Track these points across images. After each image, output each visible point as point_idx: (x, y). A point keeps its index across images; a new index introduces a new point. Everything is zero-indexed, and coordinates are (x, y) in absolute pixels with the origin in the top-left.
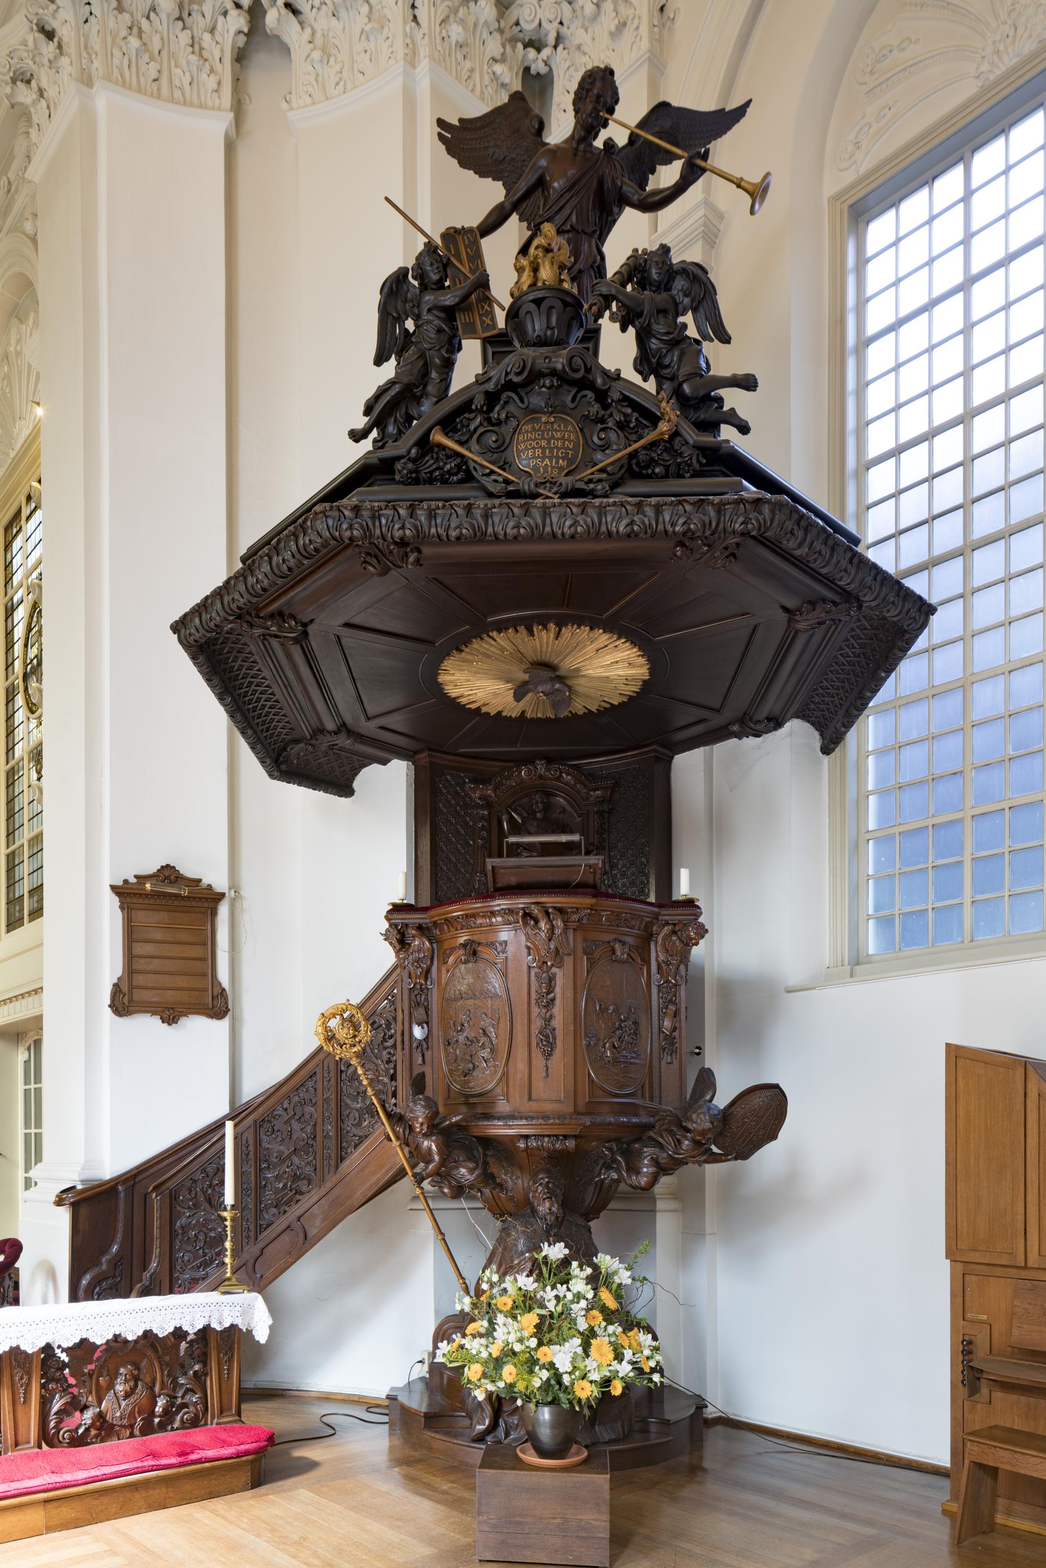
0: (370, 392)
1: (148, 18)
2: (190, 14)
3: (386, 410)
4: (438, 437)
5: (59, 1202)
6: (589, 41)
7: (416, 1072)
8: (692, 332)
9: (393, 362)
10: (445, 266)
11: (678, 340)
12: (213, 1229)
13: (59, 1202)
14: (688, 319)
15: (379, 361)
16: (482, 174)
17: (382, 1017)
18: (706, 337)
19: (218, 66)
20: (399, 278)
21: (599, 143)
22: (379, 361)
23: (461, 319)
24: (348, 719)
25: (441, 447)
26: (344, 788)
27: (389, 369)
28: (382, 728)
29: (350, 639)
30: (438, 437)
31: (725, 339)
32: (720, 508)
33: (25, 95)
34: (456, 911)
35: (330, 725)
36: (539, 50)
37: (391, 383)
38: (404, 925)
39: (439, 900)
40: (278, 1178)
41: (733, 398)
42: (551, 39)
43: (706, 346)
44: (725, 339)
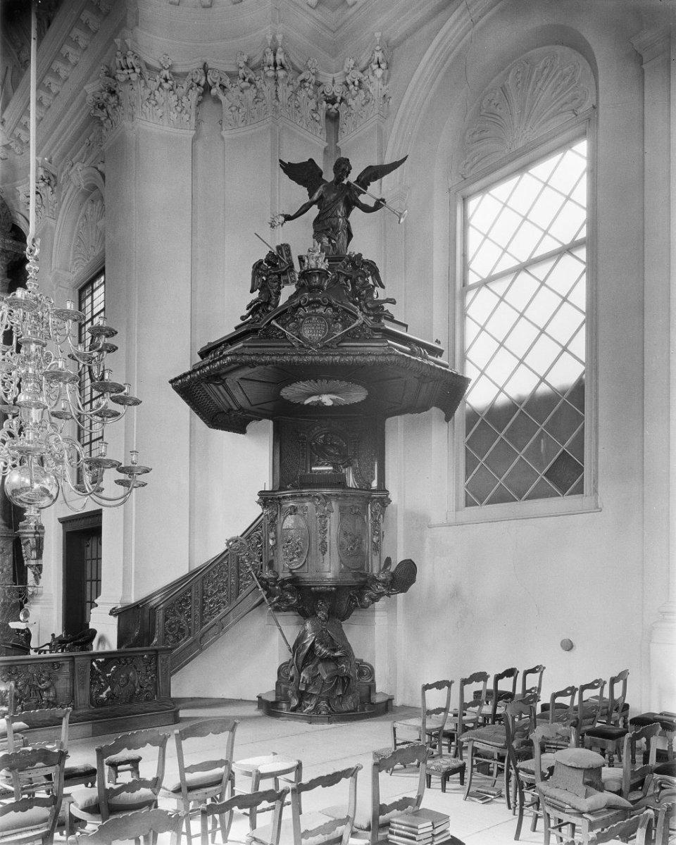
0: (249, 302)
1: (158, 90)
2: (177, 87)
3: (255, 308)
4: (274, 322)
5: (111, 613)
6: (354, 104)
7: (270, 559)
8: (371, 282)
9: (258, 291)
10: (277, 258)
11: (365, 285)
12: (182, 625)
13: (111, 613)
14: (370, 278)
15: (252, 291)
16: (299, 184)
17: (254, 534)
18: (377, 286)
19: (189, 110)
20: (260, 263)
21: (345, 182)
22: (252, 291)
23: (283, 278)
24: (243, 405)
25: (275, 326)
26: (243, 431)
27: (256, 295)
28: (259, 408)
29: (245, 385)
30: (274, 322)
31: (383, 287)
32: (44, 672)
33: (101, 114)
34: (288, 493)
35: (235, 408)
36: (333, 104)
37: (256, 301)
38: (266, 499)
39: (281, 489)
40: (211, 603)
41: (387, 306)
42: (339, 99)
43: (376, 288)
44: (383, 287)
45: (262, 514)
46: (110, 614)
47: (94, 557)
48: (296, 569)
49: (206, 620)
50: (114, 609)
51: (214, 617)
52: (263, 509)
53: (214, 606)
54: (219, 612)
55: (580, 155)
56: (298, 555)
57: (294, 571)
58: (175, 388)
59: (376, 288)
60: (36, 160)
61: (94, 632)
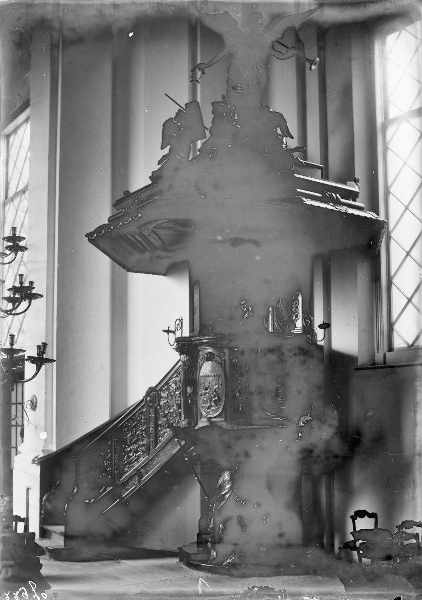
13: (34, 462)
15: (162, 148)
22: (162, 148)
45: (180, 360)
46: (33, 463)
47: (20, 401)
48: (215, 417)
49: (126, 469)
50: (37, 457)
51: (133, 467)
52: (180, 355)
53: (133, 455)
54: (138, 463)
55: (18, 270)
56: (215, 402)
57: (213, 420)
58: (90, 241)
59: (284, 138)
60: (145, 3)
61: (38, 464)
